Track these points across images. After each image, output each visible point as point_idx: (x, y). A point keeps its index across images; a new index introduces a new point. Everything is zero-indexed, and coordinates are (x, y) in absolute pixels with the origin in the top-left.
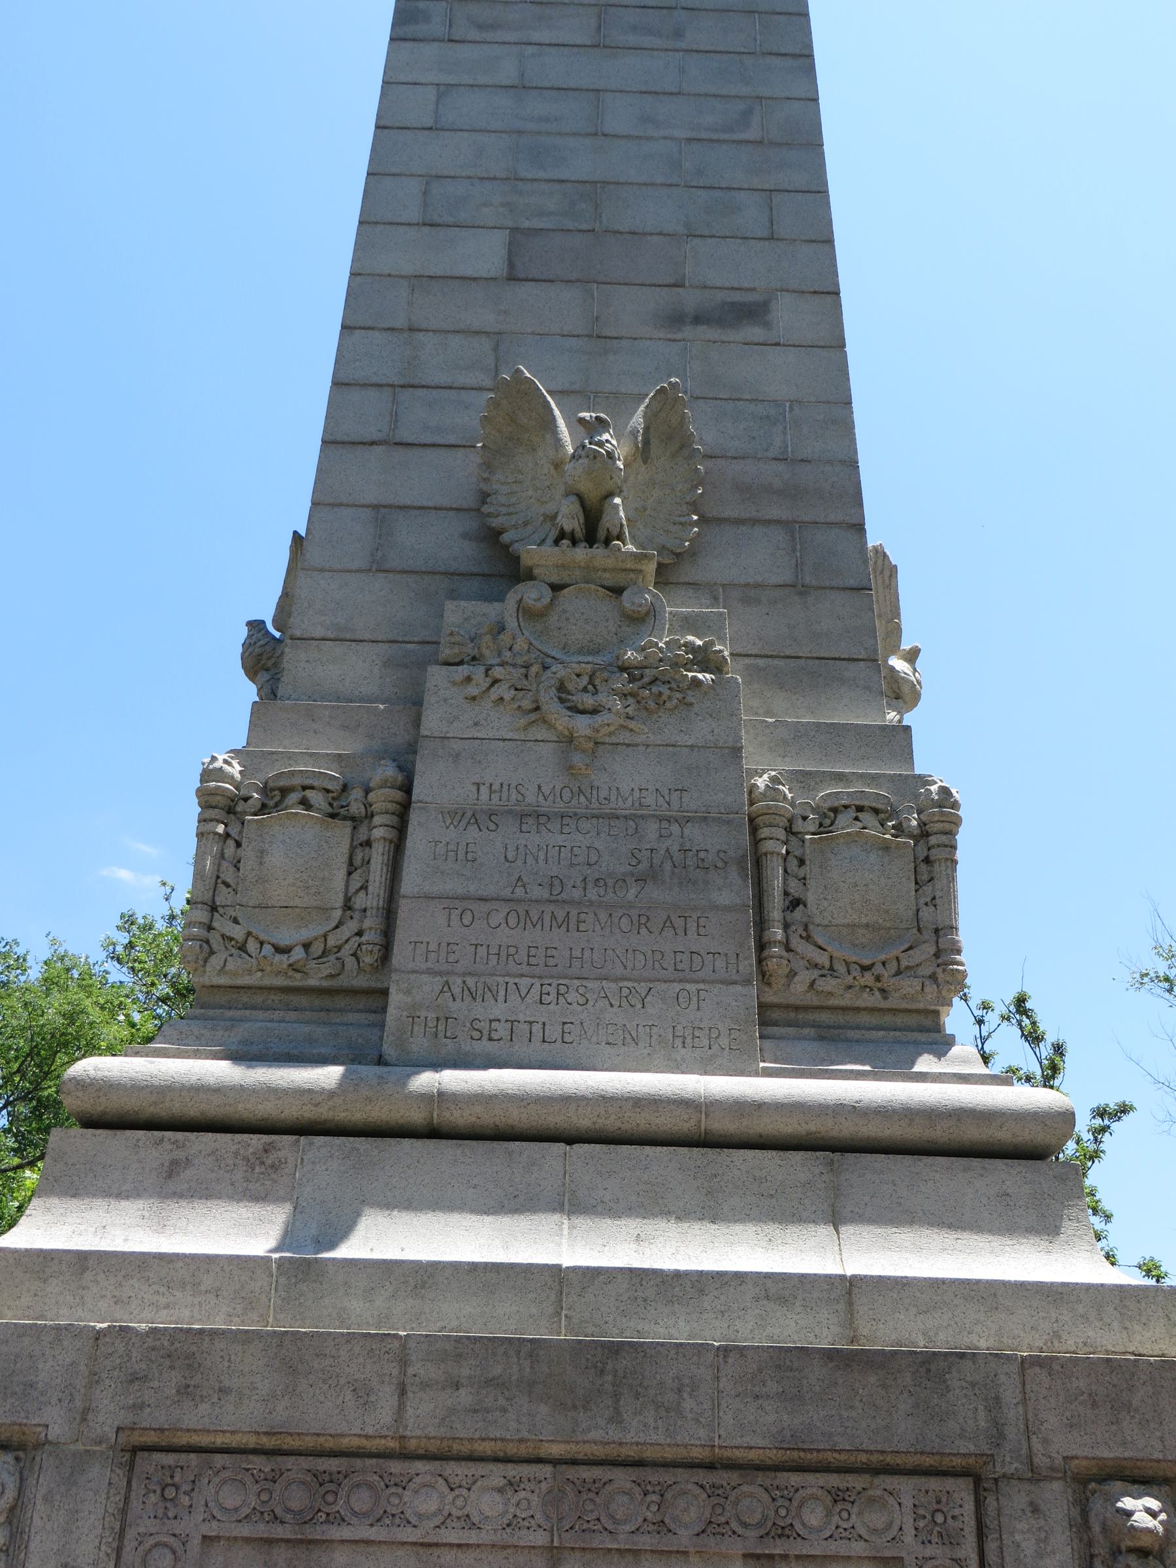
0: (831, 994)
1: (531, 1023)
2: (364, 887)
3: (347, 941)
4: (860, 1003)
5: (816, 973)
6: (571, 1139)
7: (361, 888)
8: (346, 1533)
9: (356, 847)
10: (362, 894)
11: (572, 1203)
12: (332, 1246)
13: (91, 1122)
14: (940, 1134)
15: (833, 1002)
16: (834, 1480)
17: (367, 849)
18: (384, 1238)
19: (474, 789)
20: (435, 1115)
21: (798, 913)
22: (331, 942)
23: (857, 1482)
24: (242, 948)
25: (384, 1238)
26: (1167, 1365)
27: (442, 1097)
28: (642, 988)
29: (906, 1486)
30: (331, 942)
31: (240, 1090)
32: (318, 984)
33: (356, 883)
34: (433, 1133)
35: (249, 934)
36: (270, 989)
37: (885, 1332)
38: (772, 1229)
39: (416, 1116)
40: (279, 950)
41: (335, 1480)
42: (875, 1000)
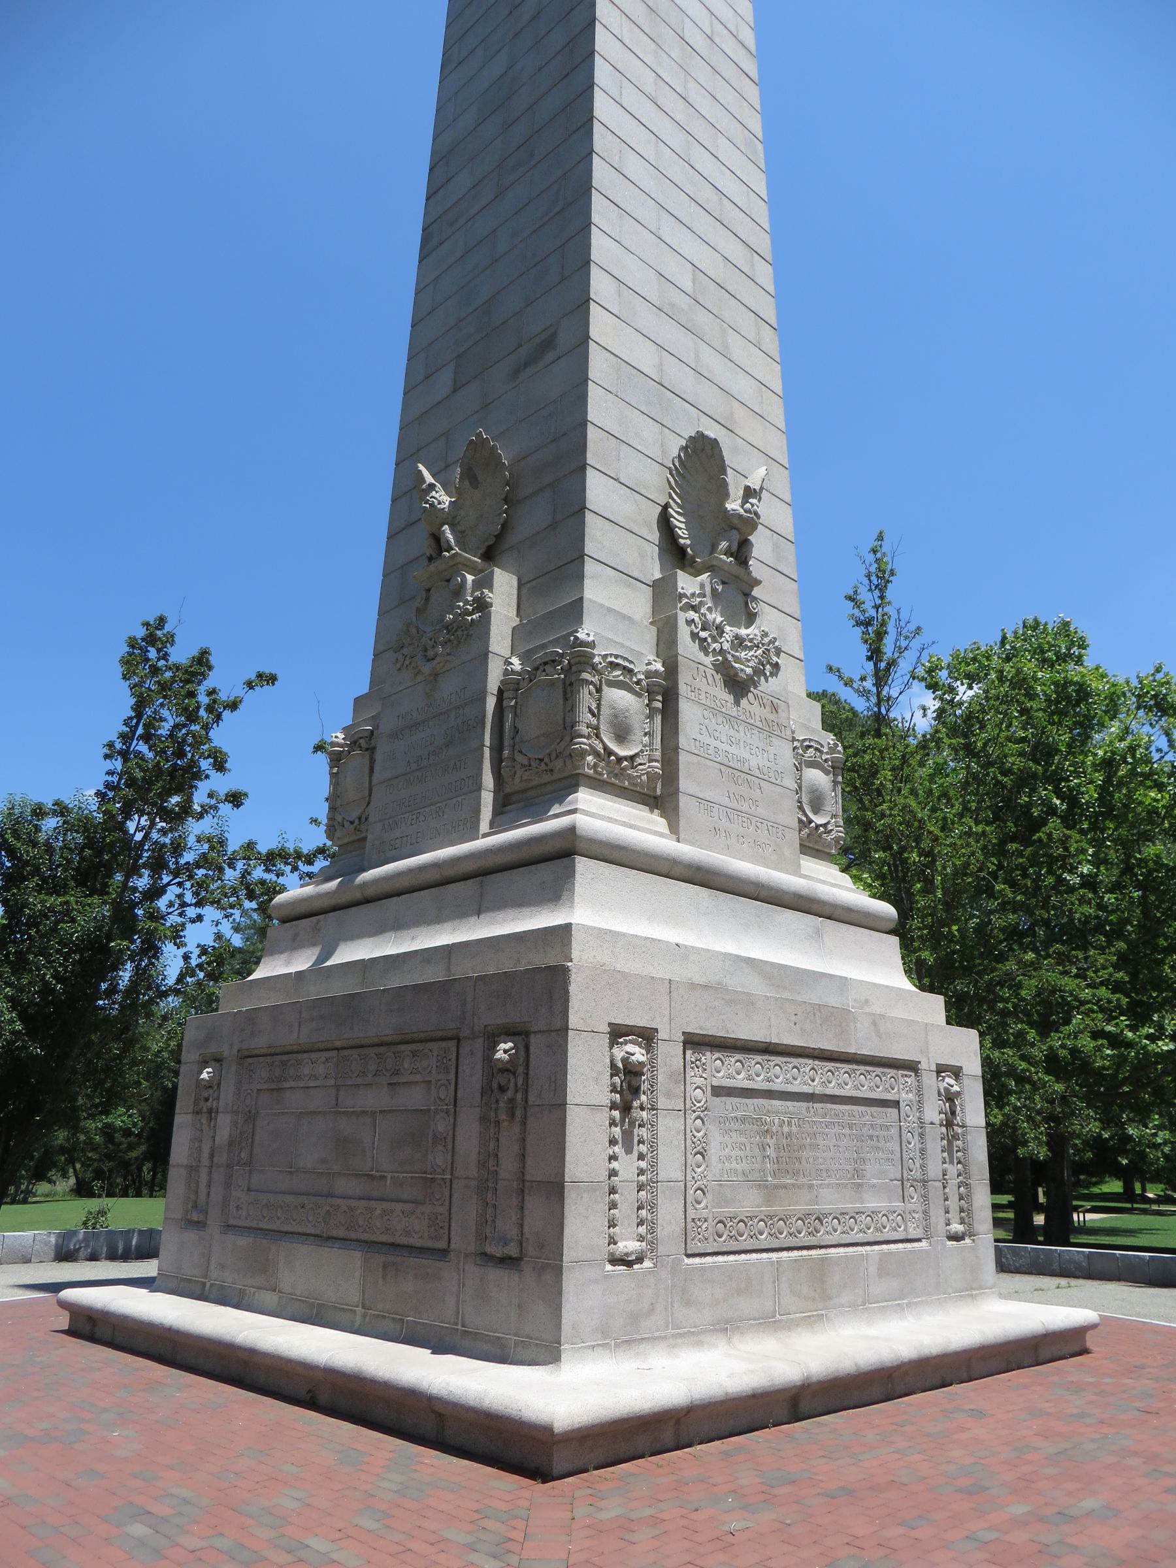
4: (543, 781)
6: (399, 894)
8: (287, 1085)
11: (398, 925)
12: (249, 974)
13: (284, 921)
14: (524, 854)
15: (532, 783)
16: (413, 1047)
18: (347, 953)
23: (420, 1046)
25: (347, 953)
26: (1175, 871)
27: (365, 884)
29: (434, 1046)
31: (319, 896)
34: (367, 901)
36: (354, 841)
37: (466, 969)
38: (456, 922)
39: (358, 895)
41: (284, 1063)
42: (547, 778)
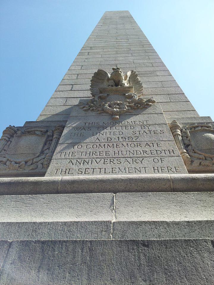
0: (208, 166)
1: (100, 169)
2: (49, 149)
3: (40, 160)
5: (201, 161)
7: (48, 149)
9: (48, 141)
10: (48, 150)
17: (51, 141)
19: (84, 124)
20: (59, 187)
21: (190, 147)
22: (35, 160)
24: (5, 164)
28: (141, 159)
30: (35, 160)
32: (28, 171)
33: (46, 148)
35: (8, 160)
40: (16, 163)
